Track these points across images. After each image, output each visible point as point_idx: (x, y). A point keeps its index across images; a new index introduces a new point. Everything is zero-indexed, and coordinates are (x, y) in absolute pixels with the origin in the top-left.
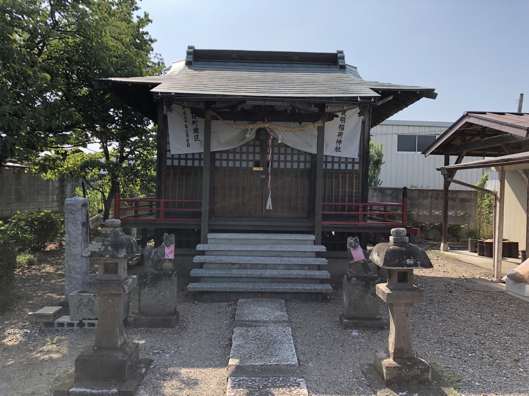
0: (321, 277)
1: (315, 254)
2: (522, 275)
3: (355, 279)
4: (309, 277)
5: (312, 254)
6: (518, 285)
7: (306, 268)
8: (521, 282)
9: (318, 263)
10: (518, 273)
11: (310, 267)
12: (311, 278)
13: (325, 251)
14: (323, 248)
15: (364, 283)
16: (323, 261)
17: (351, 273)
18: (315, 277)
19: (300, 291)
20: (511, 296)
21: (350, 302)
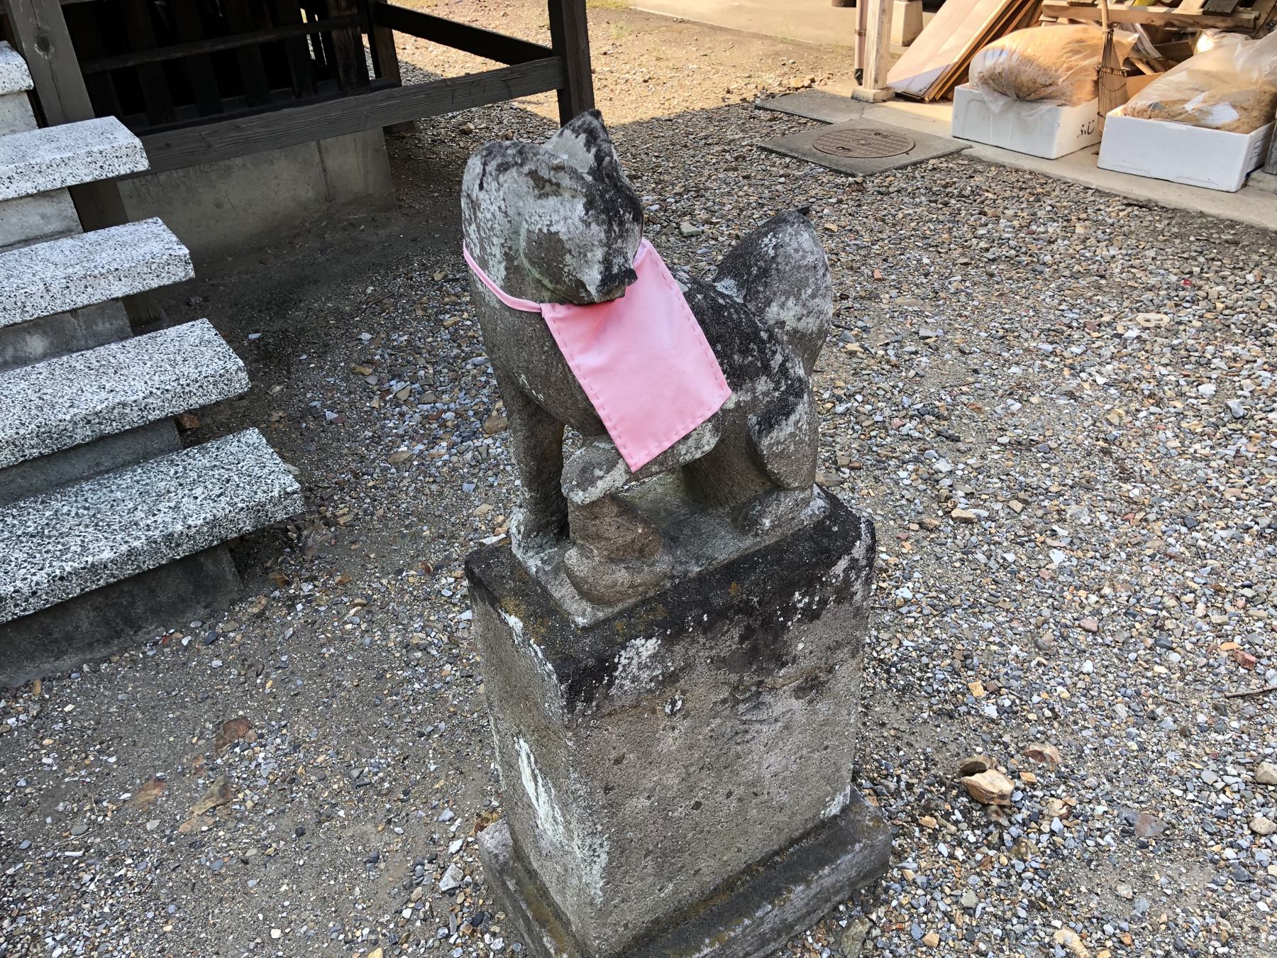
0: (179, 407)
1: (68, 206)
2: (1046, 71)
3: (648, 647)
4: (83, 434)
5: (48, 208)
6: (1026, 111)
7: (36, 344)
8: (1041, 99)
9: (120, 289)
10: (1029, 61)
11: (68, 331)
12: (101, 440)
13: (143, 164)
14: (107, 146)
15: (730, 641)
16: (147, 251)
17: (585, 593)
18: (134, 418)
19: (35, 605)
20: (1233, 224)
21: (620, 849)
